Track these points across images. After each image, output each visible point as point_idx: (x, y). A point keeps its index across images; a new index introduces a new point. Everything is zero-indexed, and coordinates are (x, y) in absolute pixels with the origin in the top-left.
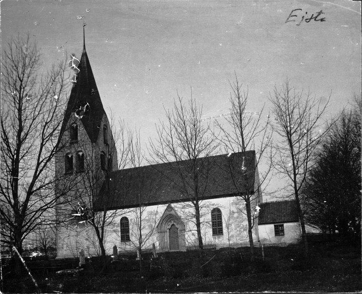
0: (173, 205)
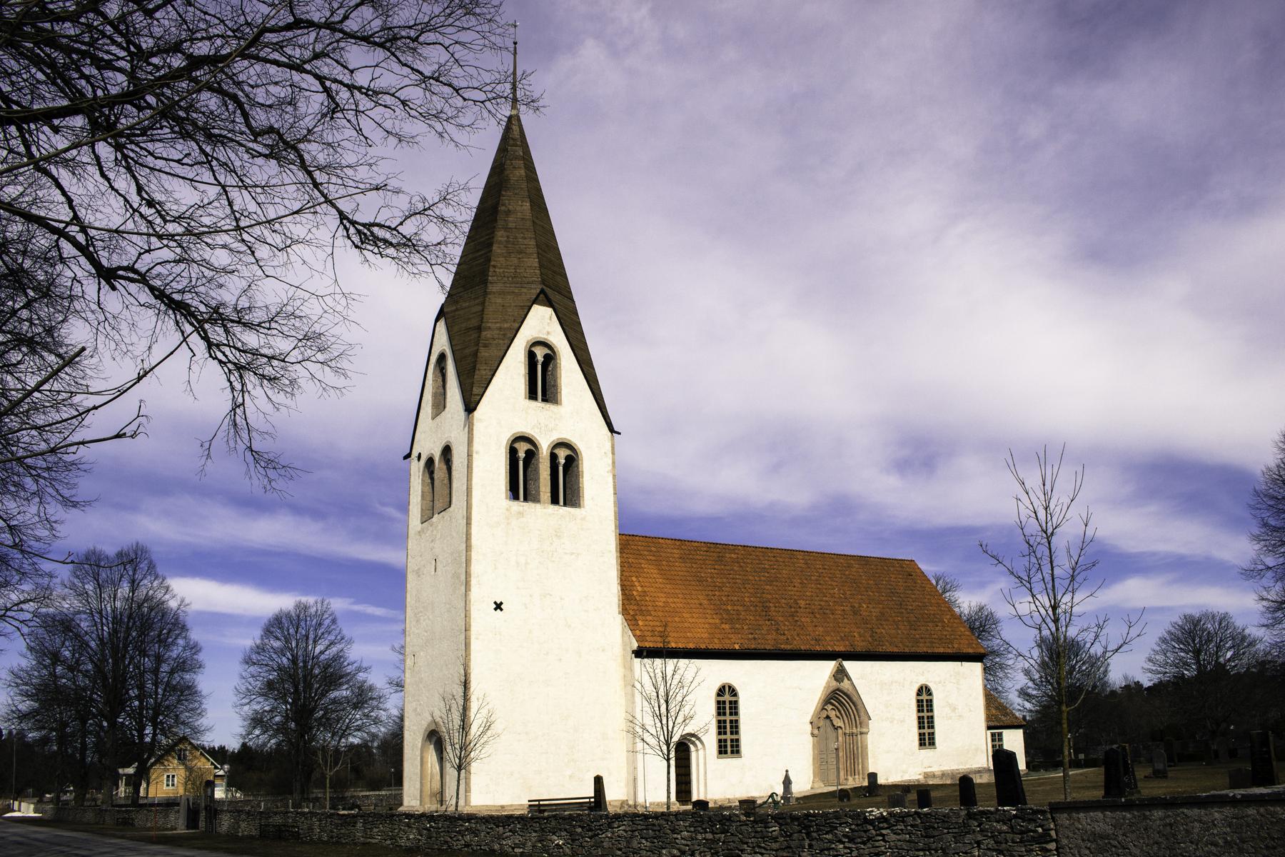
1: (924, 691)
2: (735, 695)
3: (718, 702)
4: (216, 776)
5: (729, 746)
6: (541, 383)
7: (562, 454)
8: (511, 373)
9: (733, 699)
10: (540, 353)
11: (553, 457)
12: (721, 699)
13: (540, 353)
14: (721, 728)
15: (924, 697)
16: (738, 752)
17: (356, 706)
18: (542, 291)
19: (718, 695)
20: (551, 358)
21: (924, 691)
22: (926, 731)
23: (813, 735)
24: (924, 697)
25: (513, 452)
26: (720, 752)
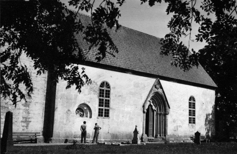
0: (163, 82)
1: (192, 98)
2: (109, 88)
14: (101, 103)
15: (105, 88)
16: (108, 116)
19: (189, 100)
21: (192, 98)
24: (192, 101)
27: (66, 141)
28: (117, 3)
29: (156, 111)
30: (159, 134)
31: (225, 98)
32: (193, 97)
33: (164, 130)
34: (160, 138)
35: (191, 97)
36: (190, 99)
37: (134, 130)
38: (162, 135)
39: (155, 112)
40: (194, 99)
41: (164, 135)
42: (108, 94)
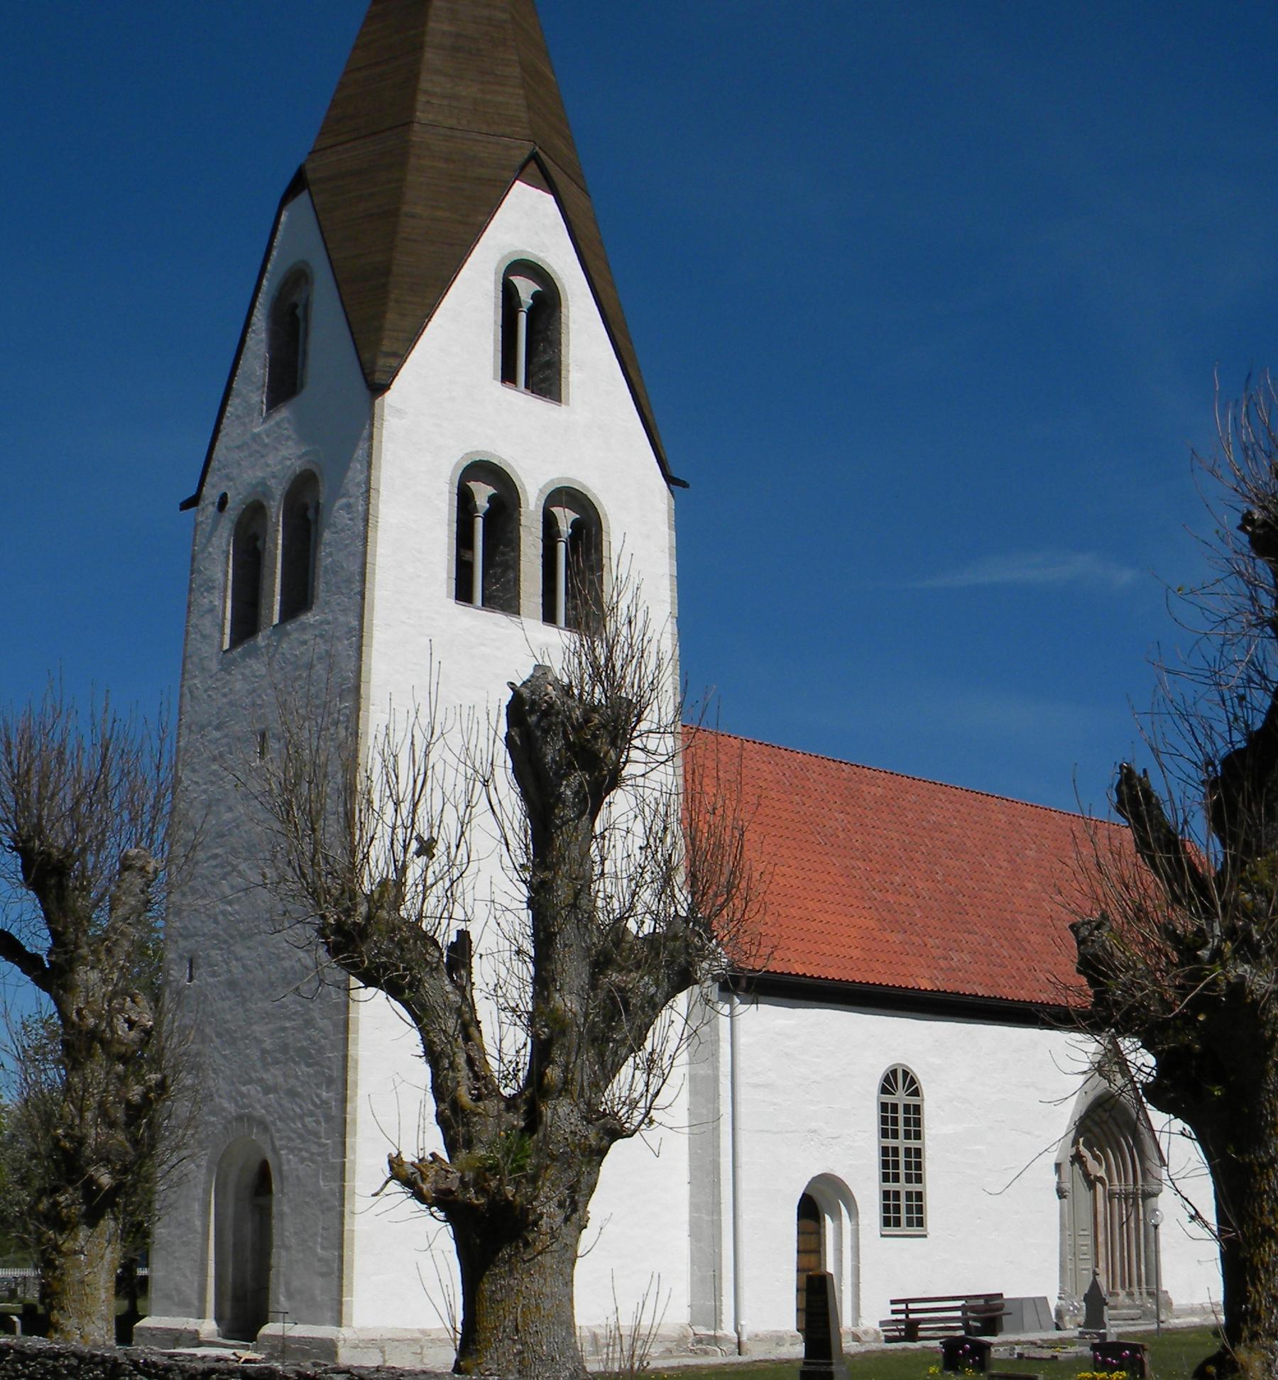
1: (899, 1081)
2: (916, 1093)
3: (884, 1107)
4: (207, 984)
5: (904, 1211)
6: (530, 353)
7: (565, 518)
8: (465, 319)
9: (912, 1101)
10: (526, 288)
11: (549, 523)
12: (888, 1099)
13: (526, 288)
14: (889, 1168)
16: (920, 1223)
17: (45, 1189)
18: (534, 157)
19: (884, 1090)
20: (549, 302)
21: (899, 1081)
22: (901, 1143)
23: (1061, 1194)
24: (900, 1097)
25: (465, 499)
26: (886, 1222)
27: (911, 1331)
28: (398, 1170)
29: (1100, 1179)
30: (1123, 1287)
31: (1201, 1018)
32: (906, 1073)
33: (1143, 1268)
34: (1129, 1307)
35: (894, 1072)
36: (889, 1082)
37: (1086, 1289)
38: (1135, 1289)
39: (1099, 1186)
40: (913, 1082)
41: (1144, 1291)
42: (914, 1126)
